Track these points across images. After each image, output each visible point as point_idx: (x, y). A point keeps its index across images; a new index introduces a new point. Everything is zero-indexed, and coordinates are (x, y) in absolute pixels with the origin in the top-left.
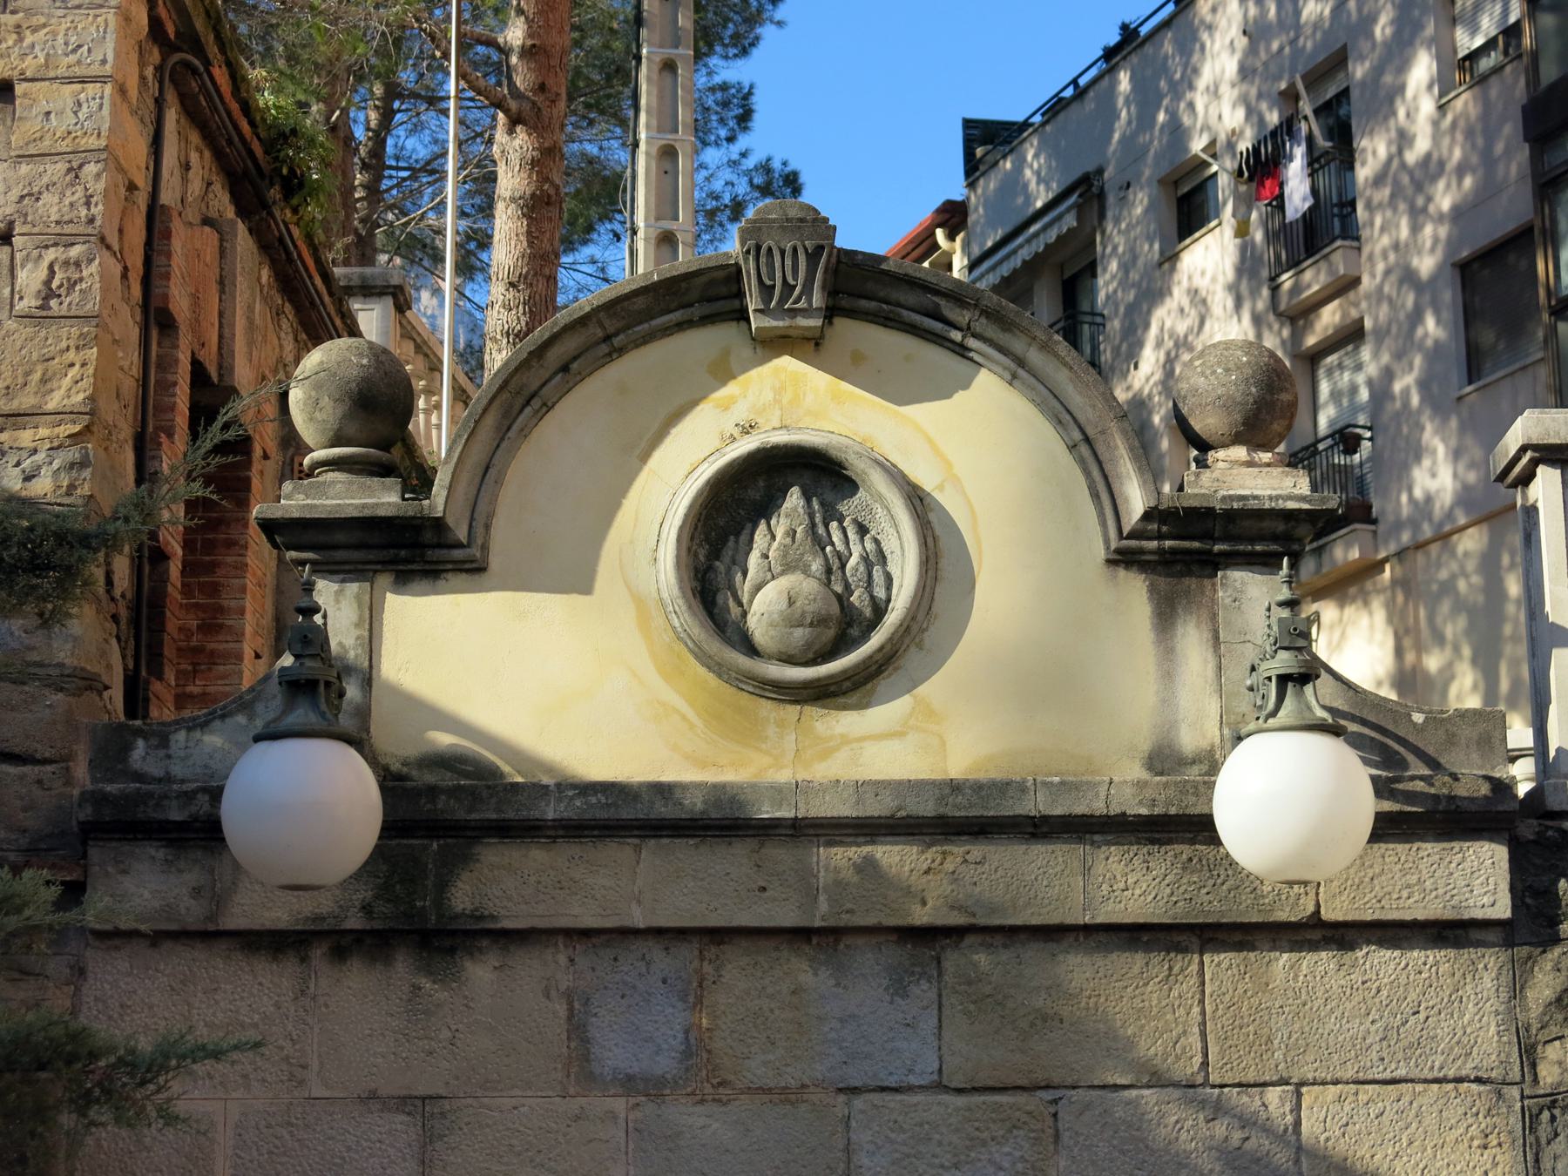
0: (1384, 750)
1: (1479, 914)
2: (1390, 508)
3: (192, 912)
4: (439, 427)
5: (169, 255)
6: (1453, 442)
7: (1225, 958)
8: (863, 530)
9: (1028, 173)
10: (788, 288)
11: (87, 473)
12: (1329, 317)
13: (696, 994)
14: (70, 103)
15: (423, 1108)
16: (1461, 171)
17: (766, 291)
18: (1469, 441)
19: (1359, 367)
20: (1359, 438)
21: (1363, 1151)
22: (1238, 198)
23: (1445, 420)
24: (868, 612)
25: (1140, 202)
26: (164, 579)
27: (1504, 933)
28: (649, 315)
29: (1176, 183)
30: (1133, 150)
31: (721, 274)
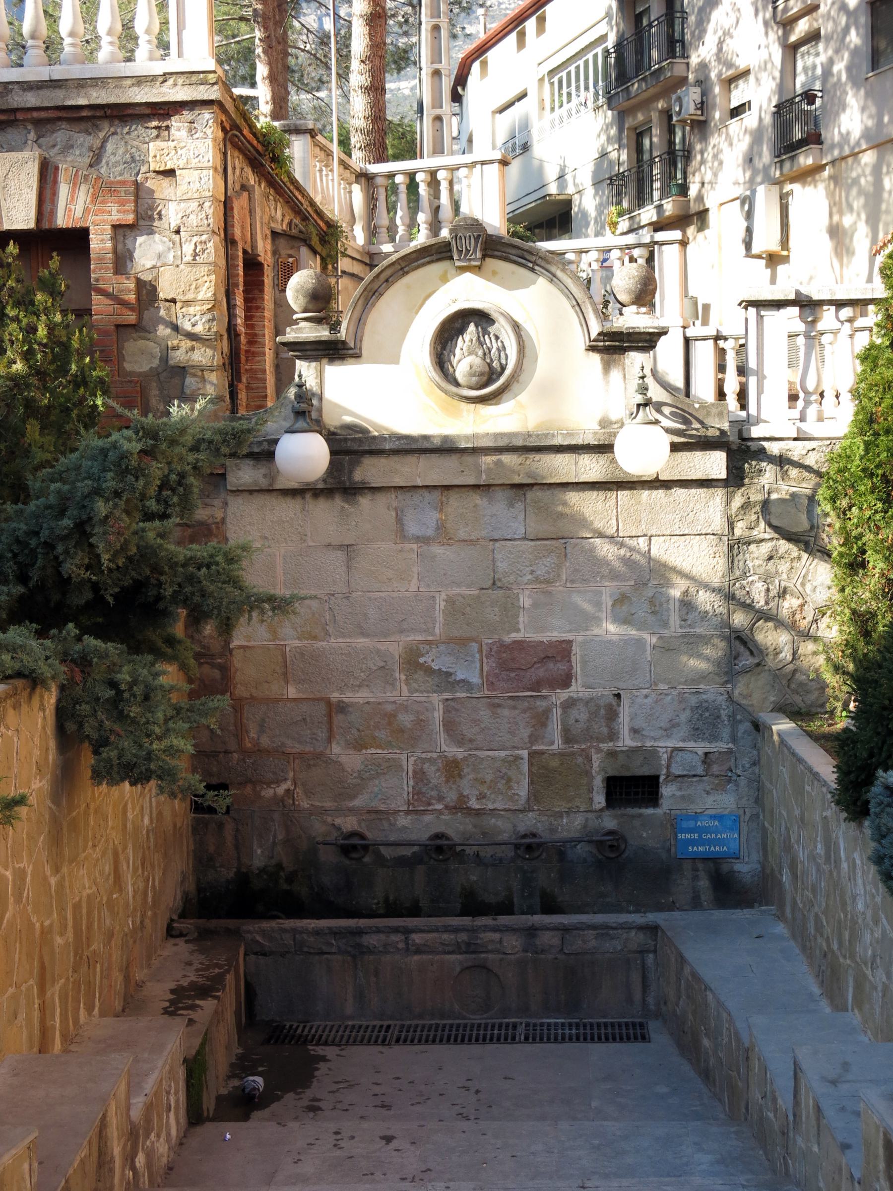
0: (684, 418)
1: (715, 477)
2: (829, 136)
3: (264, 483)
4: (333, 180)
5: (233, 217)
6: (862, 103)
7: (626, 493)
8: (497, 338)
10: (468, 251)
12: (802, 27)
14: (198, 179)
15: (347, 548)
18: (870, 103)
19: (817, 54)
20: (815, 96)
23: (858, 89)
26: (239, 343)
28: (417, 260)
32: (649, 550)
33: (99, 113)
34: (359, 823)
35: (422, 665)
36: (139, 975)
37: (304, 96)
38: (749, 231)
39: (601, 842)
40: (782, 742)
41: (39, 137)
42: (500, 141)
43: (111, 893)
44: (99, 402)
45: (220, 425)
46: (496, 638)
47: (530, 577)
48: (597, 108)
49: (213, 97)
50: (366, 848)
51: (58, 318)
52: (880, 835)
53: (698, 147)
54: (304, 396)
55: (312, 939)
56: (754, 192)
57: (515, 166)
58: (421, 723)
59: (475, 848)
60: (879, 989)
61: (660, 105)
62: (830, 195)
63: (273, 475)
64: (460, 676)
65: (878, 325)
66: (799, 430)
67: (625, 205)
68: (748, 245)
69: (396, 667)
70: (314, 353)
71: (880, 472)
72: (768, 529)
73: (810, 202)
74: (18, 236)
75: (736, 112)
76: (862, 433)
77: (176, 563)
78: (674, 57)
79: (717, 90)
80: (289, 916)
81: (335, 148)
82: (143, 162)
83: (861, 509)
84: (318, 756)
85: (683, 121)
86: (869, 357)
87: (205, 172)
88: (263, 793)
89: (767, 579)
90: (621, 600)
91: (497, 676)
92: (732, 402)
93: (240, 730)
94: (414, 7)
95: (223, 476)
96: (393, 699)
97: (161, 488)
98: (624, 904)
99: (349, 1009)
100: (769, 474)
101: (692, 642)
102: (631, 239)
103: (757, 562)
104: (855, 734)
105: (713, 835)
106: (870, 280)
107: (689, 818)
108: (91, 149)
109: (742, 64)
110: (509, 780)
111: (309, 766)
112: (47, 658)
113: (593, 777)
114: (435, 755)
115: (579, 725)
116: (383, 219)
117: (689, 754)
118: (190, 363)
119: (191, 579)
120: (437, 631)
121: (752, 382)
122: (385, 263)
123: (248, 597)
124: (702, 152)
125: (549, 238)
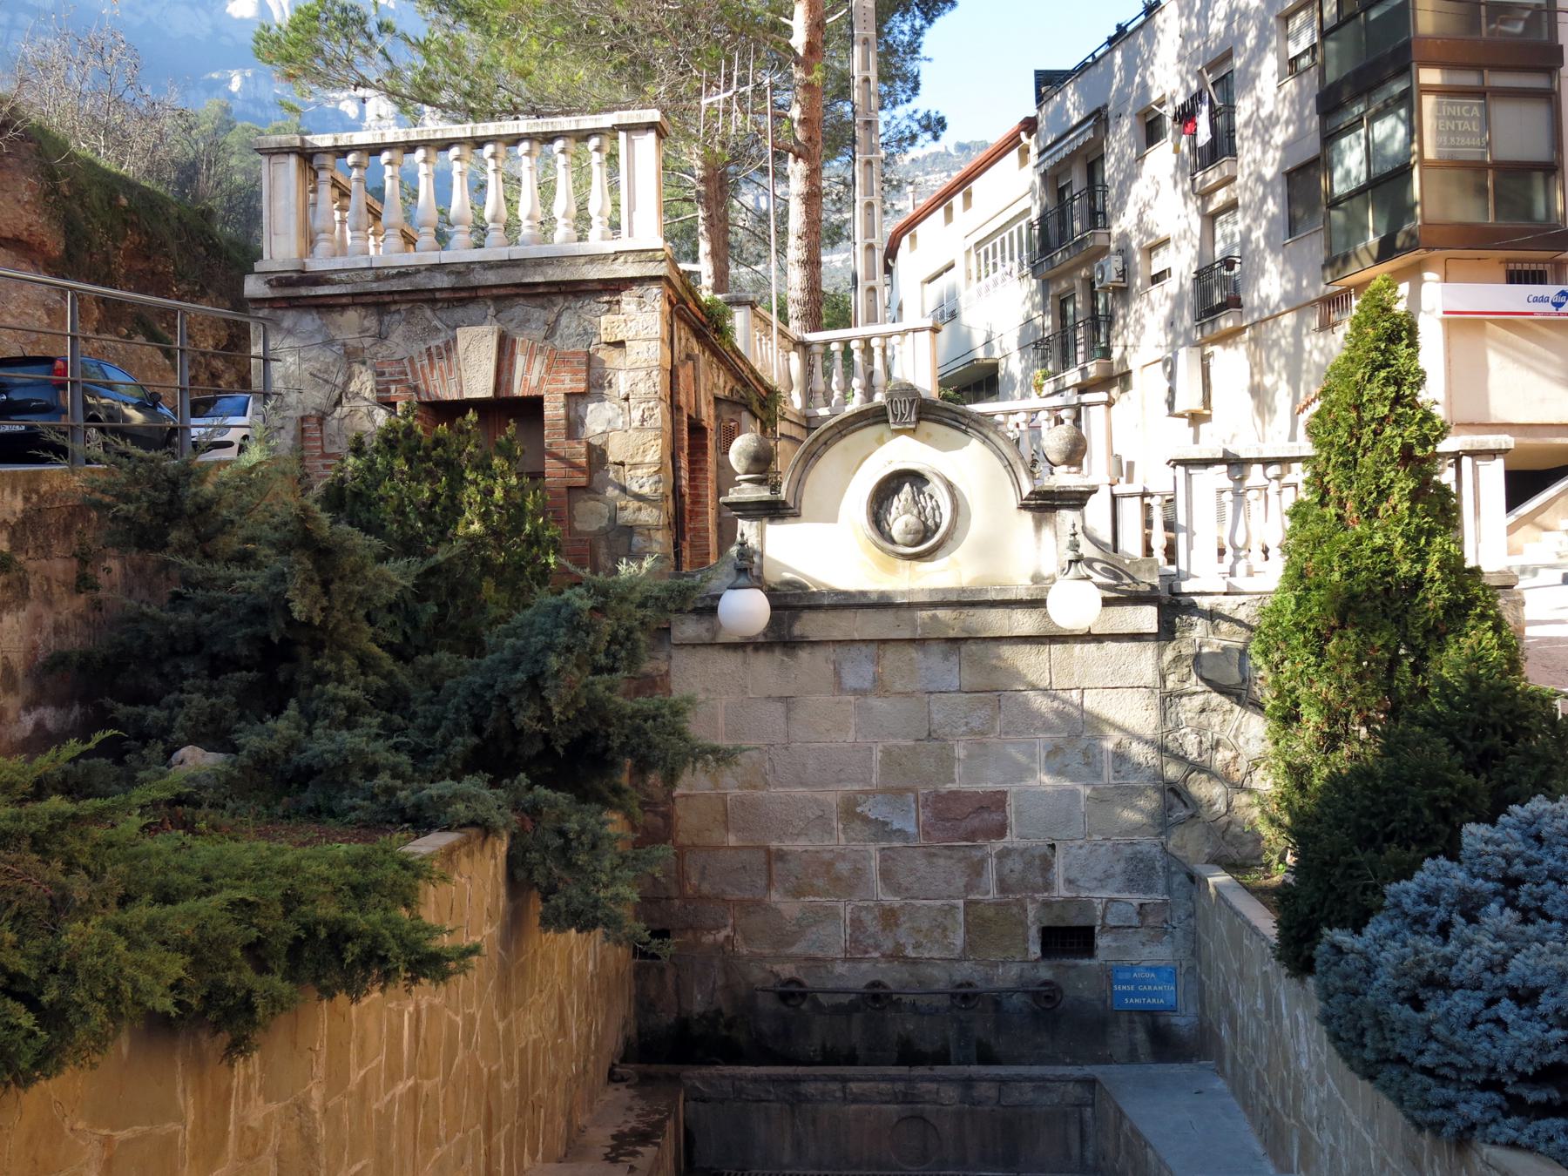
3: (706, 637)
8: (931, 497)
9: (1069, 104)
12: (1220, 197)
13: (877, 661)
15: (784, 699)
16: (1287, 123)
17: (895, 416)
18: (1288, 268)
19: (1236, 223)
22: (1175, 132)
25: (1126, 125)
27: (1156, 637)
29: (1146, 115)
30: (1123, 97)
33: (554, 290)
36: (581, 1120)
37: (743, 270)
38: (1172, 391)
40: (1219, 894)
41: (498, 312)
42: (928, 311)
43: (556, 1038)
44: (551, 560)
45: (665, 582)
48: (1022, 277)
49: (661, 273)
50: (803, 995)
51: (514, 481)
52: (1327, 995)
53: (1121, 312)
54: (746, 554)
56: (1176, 354)
57: (943, 336)
58: (858, 872)
60: (1327, 1151)
61: (1083, 273)
62: (1251, 356)
63: (716, 628)
64: (896, 826)
65: (1306, 482)
66: (1229, 585)
67: (1050, 368)
68: (1171, 404)
69: (834, 817)
71: (1312, 626)
73: (1231, 363)
74: (478, 404)
75: (1157, 279)
76: (1293, 588)
77: (624, 716)
79: (1138, 258)
80: (728, 1062)
81: (774, 318)
82: (595, 334)
83: (1293, 662)
84: (758, 903)
85: (1105, 289)
86: (1298, 513)
89: (1200, 731)
90: (1054, 751)
91: (932, 825)
92: (1159, 554)
93: (681, 876)
94: (846, 186)
95: (668, 630)
97: (610, 643)
99: (786, 1159)
100: (1200, 628)
101: (1127, 794)
102: (1057, 401)
103: (1190, 715)
104: (1296, 889)
106: (1293, 437)
108: (546, 323)
109: (1162, 233)
110: (945, 929)
112: (500, 807)
114: (871, 904)
116: (819, 382)
119: (638, 731)
121: (1182, 539)
122: (824, 426)
123: (693, 749)
124: (1124, 317)
125: (977, 400)
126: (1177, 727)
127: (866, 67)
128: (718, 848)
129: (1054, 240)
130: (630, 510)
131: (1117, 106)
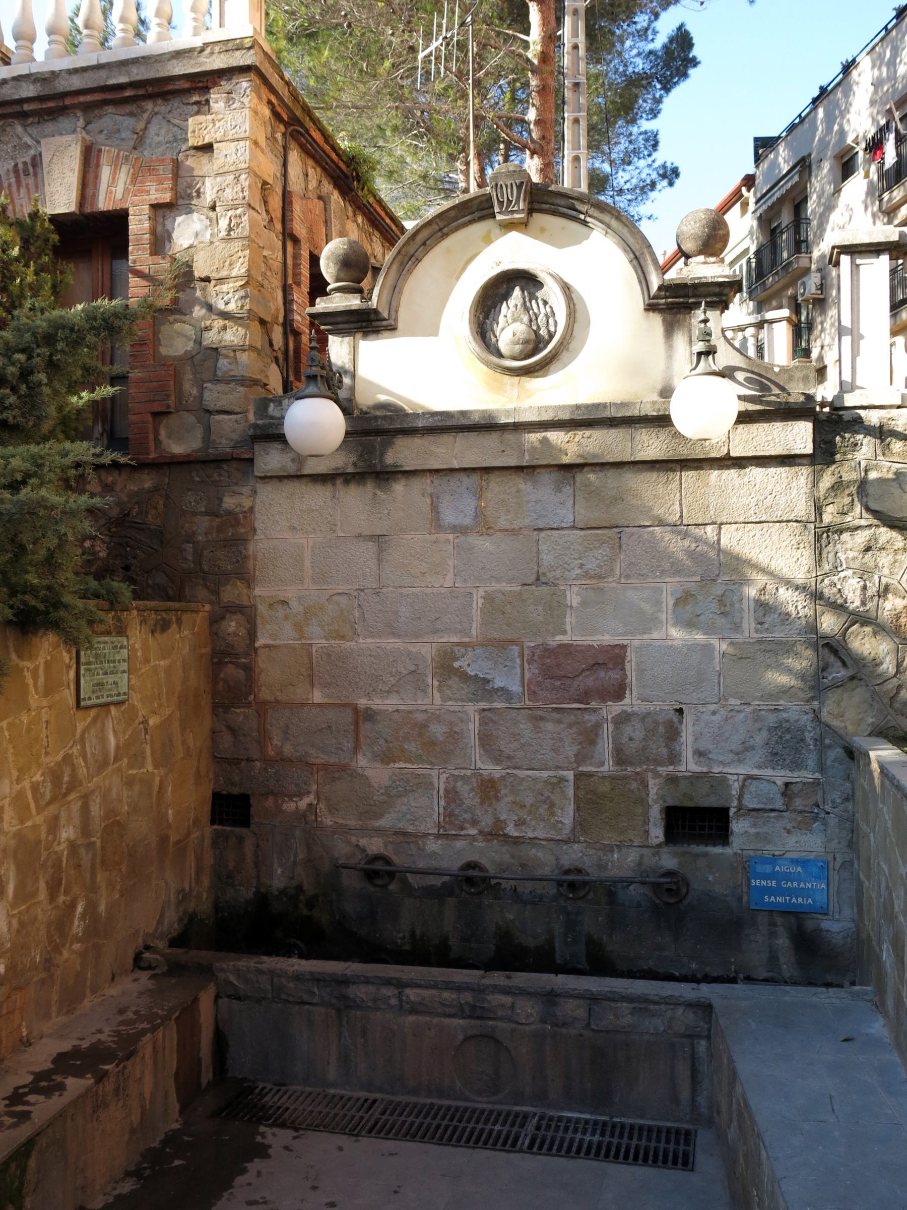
0: (761, 383)
1: (798, 452)
7: (691, 473)
8: (545, 303)
9: (780, 159)
10: (509, 202)
11: (248, 300)
15: (377, 538)
17: (501, 203)
21: (746, 551)
24: (546, 337)
25: (826, 166)
28: (456, 219)
29: (842, 157)
30: (824, 144)
31: (484, 198)
32: (719, 540)
34: (386, 845)
35: (457, 670)
39: (658, 885)
41: (88, 123)
46: (539, 640)
47: (579, 571)
50: (391, 875)
53: (819, 320)
55: (291, 985)
58: (454, 736)
59: (512, 883)
61: (790, 292)
64: (498, 684)
69: (429, 672)
70: (346, 326)
72: (865, 514)
78: (800, 253)
84: (343, 768)
85: (806, 301)
87: (242, 143)
88: (285, 807)
89: (864, 573)
90: (684, 599)
91: (539, 684)
95: (251, 461)
96: (424, 708)
98: (685, 960)
99: (332, 1074)
100: (867, 447)
101: (776, 650)
103: (851, 554)
105: (795, 884)
107: (765, 861)
111: (334, 779)
113: (649, 807)
114: (469, 773)
115: (633, 745)
117: (765, 783)
118: (223, 344)
120: (474, 632)
124: (822, 323)
126: (835, 569)
127: (575, 34)
128: (302, 705)
129: (766, 262)
130: (215, 330)
131: (818, 153)
